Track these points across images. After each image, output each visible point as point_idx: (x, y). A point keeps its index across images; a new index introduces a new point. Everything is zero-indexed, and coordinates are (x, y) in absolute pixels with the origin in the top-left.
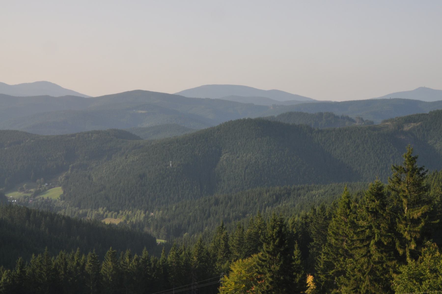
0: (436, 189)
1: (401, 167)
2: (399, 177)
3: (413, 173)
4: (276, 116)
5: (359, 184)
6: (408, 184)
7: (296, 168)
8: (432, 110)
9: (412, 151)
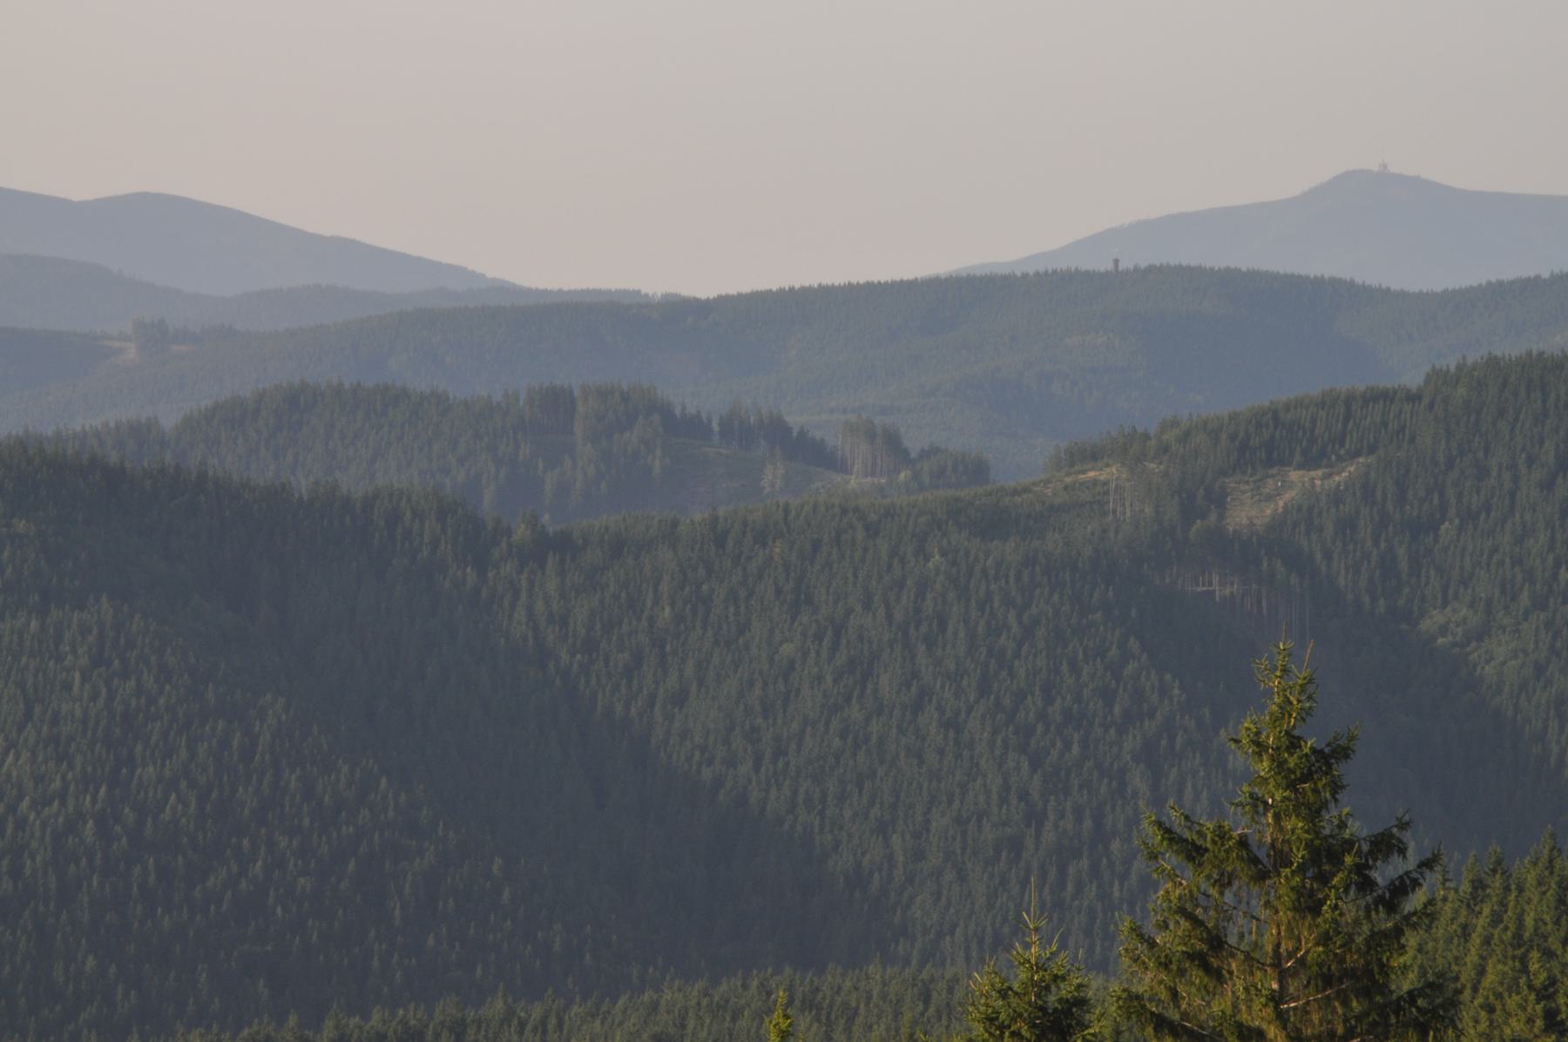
0: (1498, 1016)
1: (1222, 835)
2: (1212, 913)
3: (1324, 879)
4: (169, 421)
5: (885, 984)
6: (1282, 976)
7: (352, 866)
8: (1451, 363)
9: (1310, 698)
